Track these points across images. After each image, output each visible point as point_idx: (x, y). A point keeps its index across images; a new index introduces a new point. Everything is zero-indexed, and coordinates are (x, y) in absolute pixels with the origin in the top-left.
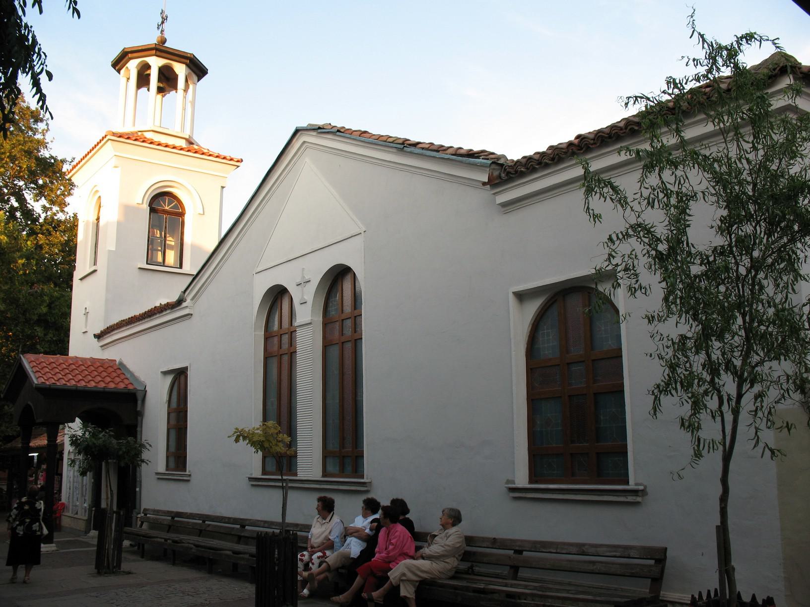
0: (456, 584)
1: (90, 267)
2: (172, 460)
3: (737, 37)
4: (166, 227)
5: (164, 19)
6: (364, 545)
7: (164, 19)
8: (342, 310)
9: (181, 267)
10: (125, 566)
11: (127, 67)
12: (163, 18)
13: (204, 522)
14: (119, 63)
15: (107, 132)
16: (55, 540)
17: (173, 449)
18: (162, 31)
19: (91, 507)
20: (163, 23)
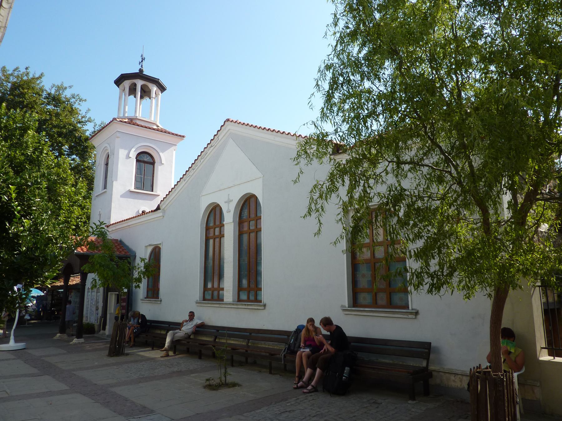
0: (239, 343)
1: (102, 190)
2: (150, 293)
3: (40, 77)
4: (144, 170)
5: (143, 59)
6: (429, 369)
7: (143, 59)
8: (250, 217)
9: (152, 191)
10: (126, 351)
11: (123, 85)
12: (142, 59)
13: (170, 325)
14: (118, 82)
15: (113, 118)
16: (83, 336)
17: (150, 287)
18: (142, 66)
19: (101, 318)
20: (142, 61)
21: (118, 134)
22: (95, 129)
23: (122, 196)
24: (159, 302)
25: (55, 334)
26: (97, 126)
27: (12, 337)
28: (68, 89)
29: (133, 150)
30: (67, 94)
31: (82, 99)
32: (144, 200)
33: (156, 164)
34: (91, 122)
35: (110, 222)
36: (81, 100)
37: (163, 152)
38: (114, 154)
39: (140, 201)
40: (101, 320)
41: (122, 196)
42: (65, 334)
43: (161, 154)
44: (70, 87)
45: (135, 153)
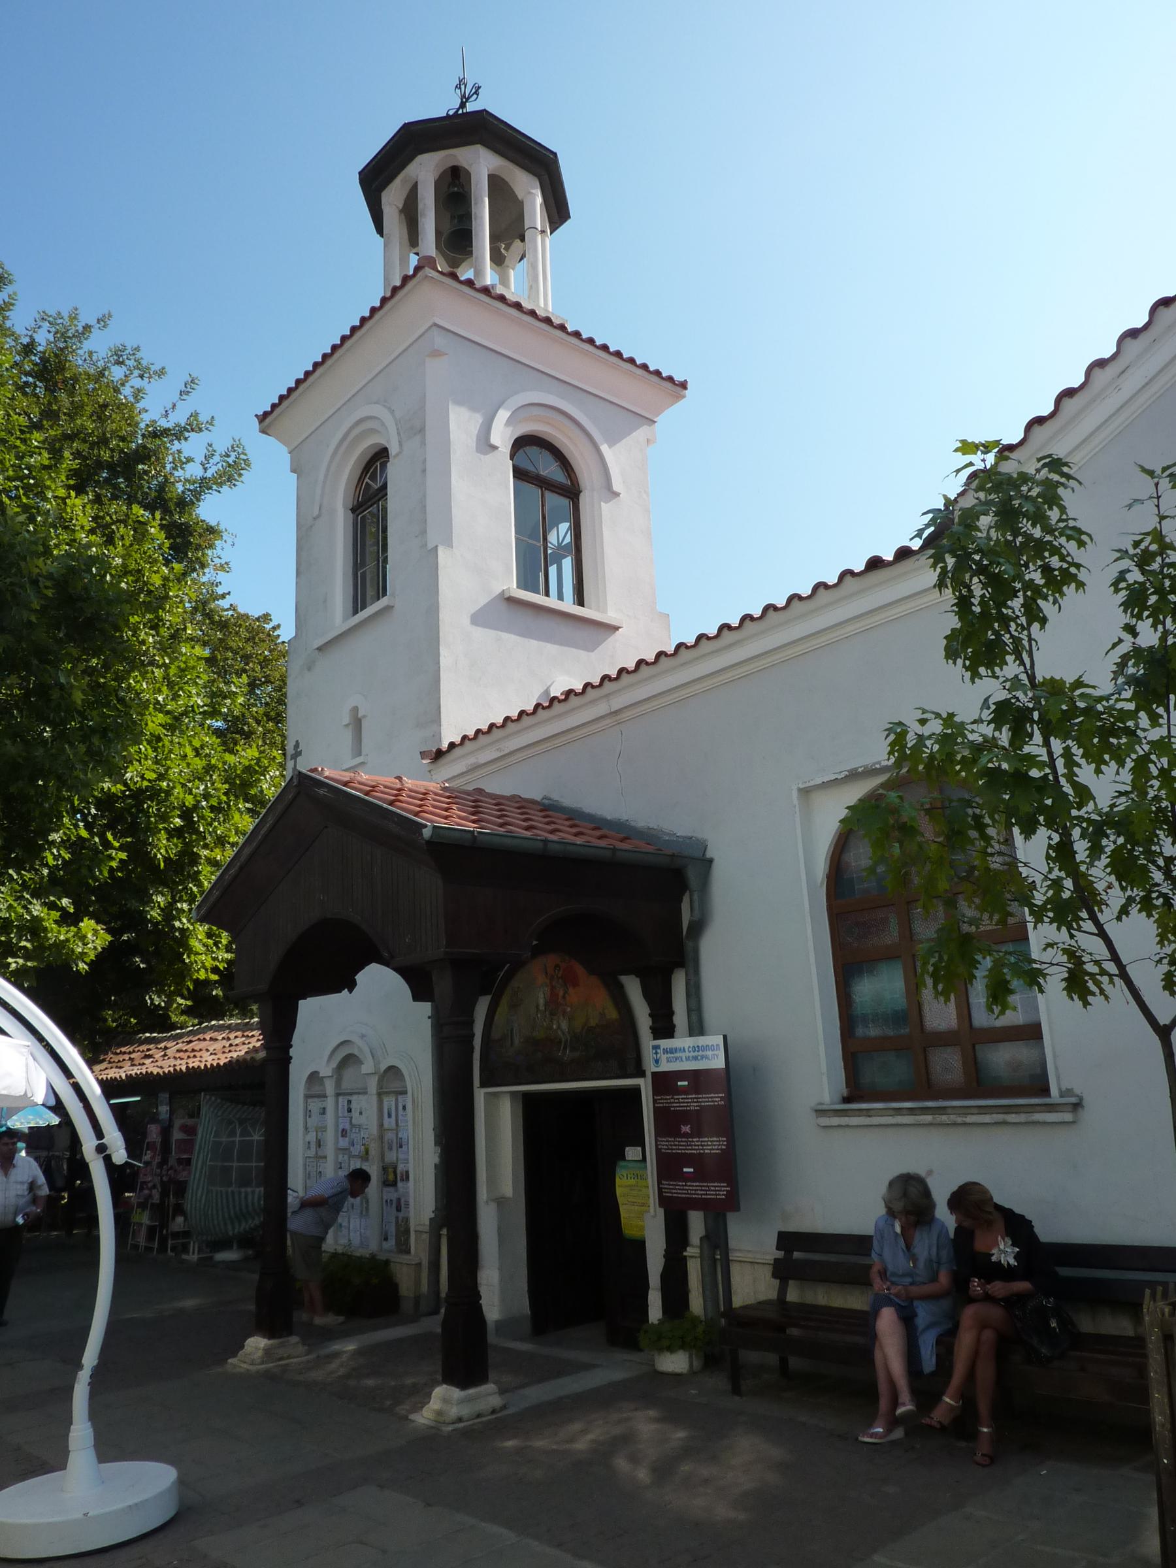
1: (345, 619)
21: (439, 341)
22: (205, 469)
23: (479, 619)
24: (1068, 1117)
25: (421, 1394)
26: (217, 458)
27: (81, 1432)
28: (96, 333)
29: (503, 415)
30: (98, 345)
31: (148, 368)
32: (561, 644)
33: (585, 500)
34: (200, 430)
35: (438, 736)
36: (144, 372)
37: (612, 443)
38: (422, 430)
39: (551, 649)
40: (439, 1236)
41: (479, 619)
42: (294, 1339)
43: (604, 448)
44: (103, 321)
45: (510, 429)
